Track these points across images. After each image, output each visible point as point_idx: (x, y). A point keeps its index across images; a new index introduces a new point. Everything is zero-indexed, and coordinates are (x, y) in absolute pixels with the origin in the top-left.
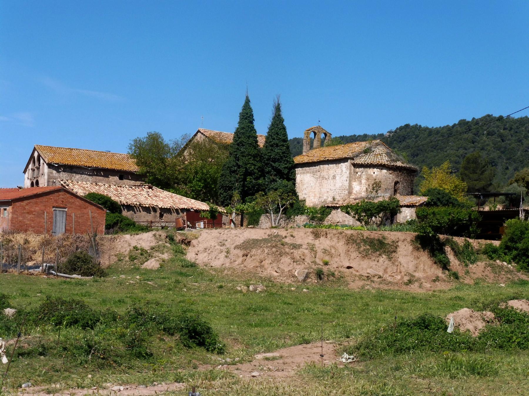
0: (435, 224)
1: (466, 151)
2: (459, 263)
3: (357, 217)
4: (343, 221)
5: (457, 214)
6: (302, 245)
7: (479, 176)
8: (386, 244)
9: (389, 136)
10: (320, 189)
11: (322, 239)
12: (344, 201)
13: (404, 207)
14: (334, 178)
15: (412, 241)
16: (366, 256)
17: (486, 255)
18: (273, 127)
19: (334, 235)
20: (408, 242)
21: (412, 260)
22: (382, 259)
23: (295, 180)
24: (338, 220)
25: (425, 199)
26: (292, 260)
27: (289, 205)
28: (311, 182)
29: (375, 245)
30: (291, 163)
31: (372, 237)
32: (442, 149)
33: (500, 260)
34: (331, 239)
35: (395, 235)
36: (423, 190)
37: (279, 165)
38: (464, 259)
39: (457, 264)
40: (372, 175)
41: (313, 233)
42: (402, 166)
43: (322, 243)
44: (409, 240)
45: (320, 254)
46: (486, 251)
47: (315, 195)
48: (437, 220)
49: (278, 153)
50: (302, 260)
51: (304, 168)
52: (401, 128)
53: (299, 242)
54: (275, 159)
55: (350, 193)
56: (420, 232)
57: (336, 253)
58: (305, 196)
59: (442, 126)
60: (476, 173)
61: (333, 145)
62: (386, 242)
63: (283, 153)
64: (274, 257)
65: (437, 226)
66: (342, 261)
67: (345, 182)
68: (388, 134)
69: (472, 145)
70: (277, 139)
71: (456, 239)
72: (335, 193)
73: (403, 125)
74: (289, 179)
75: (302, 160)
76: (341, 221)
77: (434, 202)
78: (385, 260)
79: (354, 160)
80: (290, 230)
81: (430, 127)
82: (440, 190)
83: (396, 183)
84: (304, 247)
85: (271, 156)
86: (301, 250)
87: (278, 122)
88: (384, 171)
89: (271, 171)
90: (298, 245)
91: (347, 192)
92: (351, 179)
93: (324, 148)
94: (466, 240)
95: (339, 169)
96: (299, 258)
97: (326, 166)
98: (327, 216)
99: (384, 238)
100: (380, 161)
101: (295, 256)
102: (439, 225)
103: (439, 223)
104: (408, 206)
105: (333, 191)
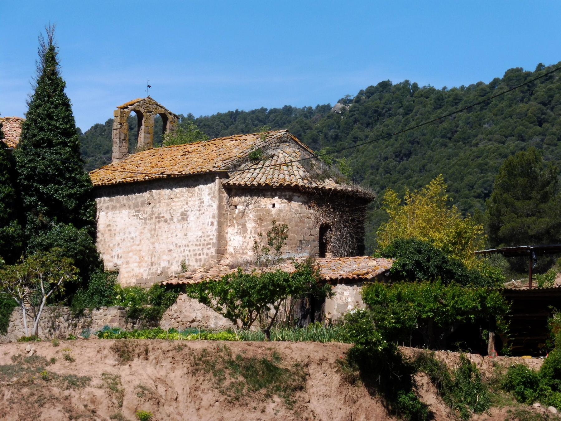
0: (389, 322)
1: (523, 144)
2: (448, 410)
3: (225, 311)
4: (204, 317)
5: (453, 298)
6: (89, 379)
7: (537, 205)
8: (282, 370)
9: (343, 109)
10: (153, 243)
11: (136, 362)
12: (207, 271)
13: (341, 283)
14: (183, 219)
15: (339, 362)
16: (237, 399)
17: (512, 392)
18: (39, 102)
19: (164, 352)
20: (330, 364)
21: (339, 406)
22: (272, 405)
23: (93, 224)
24: (193, 316)
25: (386, 264)
26: (67, 415)
27: (64, 286)
28: (132, 229)
29: (257, 374)
30: (84, 186)
31: (250, 355)
32: (466, 140)
33: (542, 403)
34: (157, 363)
35: (302, 349)
36: (385, 243)
37: (57, 191)
38: (461, 401)
39: (444, 413)
40: (268, 212)
41: (116, 349)
42: (336, 189)
43: (136, 371)
44: (332, 360)
45: (131, 399)
46: (511, 382)
47: (141, 257)
48: (394, 314)
49: (51, 161)
50: (88, 413)
51: (114, 198)
52: (370, 92)
53: (83, 371)
54: (46, 175)
55: (221, 252)
56: (357, 342)
57: (169, 393)
58: (119, 262)
59: (467, 85)
60: (530, 198)
61: (183, 142)
62: (281, 366)
63: (63, 162)
64: (25, 407)
65: (395, 328)
66: (181, 411)
67: (209, 228)
68: (340, 106)
69: (538, 128)
70: (51, 130)
71: (440, 356)
72: (187, 253)
73: (375, 84)
74: (79, 224)
75: (109, 177)
76: (199, 317)
77: (407, 271)
78: (278, 408)
79: (228, 177)
80: (63, 345)
81: (438, 87)
82: (421, 243)
83: (324, 229)
84: (95, 382)
85: (35, 168)
86: (88, 389)
87: (51, 90)
88: (295, 205)
89: (37, 205)
90: (82, 378)
91: (213, 250)
92: (222, 220)
93: (162, 150)
94: (462, 358)
95: (193, 199)
96: (82, 408)
97: (166, 192)
98: (167, 307)
99: (278, 358)
100: (287, 177)
101: (73, 405)
102: (399, 326)
103: (398, 321)
104: (348, 282)
105: (182, 249)
